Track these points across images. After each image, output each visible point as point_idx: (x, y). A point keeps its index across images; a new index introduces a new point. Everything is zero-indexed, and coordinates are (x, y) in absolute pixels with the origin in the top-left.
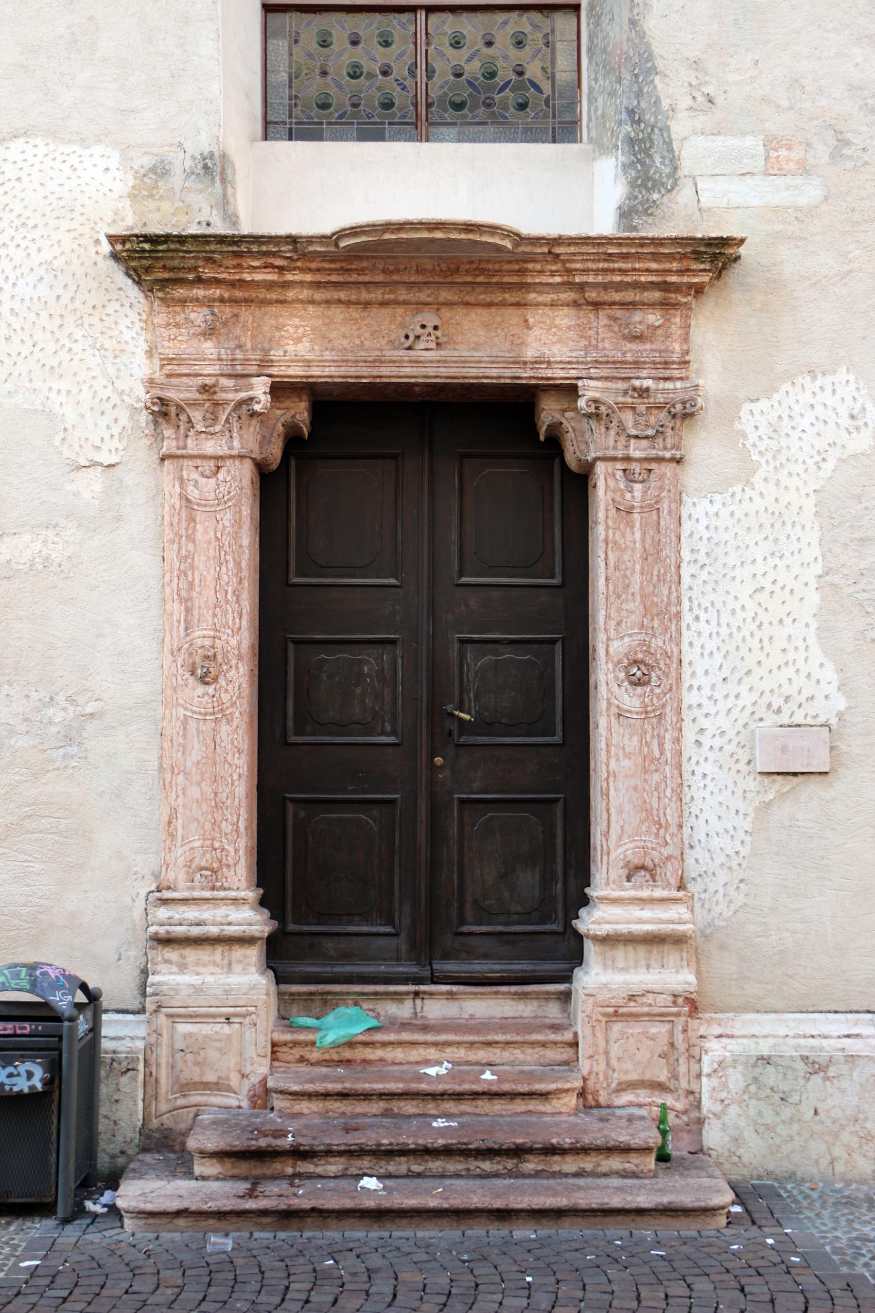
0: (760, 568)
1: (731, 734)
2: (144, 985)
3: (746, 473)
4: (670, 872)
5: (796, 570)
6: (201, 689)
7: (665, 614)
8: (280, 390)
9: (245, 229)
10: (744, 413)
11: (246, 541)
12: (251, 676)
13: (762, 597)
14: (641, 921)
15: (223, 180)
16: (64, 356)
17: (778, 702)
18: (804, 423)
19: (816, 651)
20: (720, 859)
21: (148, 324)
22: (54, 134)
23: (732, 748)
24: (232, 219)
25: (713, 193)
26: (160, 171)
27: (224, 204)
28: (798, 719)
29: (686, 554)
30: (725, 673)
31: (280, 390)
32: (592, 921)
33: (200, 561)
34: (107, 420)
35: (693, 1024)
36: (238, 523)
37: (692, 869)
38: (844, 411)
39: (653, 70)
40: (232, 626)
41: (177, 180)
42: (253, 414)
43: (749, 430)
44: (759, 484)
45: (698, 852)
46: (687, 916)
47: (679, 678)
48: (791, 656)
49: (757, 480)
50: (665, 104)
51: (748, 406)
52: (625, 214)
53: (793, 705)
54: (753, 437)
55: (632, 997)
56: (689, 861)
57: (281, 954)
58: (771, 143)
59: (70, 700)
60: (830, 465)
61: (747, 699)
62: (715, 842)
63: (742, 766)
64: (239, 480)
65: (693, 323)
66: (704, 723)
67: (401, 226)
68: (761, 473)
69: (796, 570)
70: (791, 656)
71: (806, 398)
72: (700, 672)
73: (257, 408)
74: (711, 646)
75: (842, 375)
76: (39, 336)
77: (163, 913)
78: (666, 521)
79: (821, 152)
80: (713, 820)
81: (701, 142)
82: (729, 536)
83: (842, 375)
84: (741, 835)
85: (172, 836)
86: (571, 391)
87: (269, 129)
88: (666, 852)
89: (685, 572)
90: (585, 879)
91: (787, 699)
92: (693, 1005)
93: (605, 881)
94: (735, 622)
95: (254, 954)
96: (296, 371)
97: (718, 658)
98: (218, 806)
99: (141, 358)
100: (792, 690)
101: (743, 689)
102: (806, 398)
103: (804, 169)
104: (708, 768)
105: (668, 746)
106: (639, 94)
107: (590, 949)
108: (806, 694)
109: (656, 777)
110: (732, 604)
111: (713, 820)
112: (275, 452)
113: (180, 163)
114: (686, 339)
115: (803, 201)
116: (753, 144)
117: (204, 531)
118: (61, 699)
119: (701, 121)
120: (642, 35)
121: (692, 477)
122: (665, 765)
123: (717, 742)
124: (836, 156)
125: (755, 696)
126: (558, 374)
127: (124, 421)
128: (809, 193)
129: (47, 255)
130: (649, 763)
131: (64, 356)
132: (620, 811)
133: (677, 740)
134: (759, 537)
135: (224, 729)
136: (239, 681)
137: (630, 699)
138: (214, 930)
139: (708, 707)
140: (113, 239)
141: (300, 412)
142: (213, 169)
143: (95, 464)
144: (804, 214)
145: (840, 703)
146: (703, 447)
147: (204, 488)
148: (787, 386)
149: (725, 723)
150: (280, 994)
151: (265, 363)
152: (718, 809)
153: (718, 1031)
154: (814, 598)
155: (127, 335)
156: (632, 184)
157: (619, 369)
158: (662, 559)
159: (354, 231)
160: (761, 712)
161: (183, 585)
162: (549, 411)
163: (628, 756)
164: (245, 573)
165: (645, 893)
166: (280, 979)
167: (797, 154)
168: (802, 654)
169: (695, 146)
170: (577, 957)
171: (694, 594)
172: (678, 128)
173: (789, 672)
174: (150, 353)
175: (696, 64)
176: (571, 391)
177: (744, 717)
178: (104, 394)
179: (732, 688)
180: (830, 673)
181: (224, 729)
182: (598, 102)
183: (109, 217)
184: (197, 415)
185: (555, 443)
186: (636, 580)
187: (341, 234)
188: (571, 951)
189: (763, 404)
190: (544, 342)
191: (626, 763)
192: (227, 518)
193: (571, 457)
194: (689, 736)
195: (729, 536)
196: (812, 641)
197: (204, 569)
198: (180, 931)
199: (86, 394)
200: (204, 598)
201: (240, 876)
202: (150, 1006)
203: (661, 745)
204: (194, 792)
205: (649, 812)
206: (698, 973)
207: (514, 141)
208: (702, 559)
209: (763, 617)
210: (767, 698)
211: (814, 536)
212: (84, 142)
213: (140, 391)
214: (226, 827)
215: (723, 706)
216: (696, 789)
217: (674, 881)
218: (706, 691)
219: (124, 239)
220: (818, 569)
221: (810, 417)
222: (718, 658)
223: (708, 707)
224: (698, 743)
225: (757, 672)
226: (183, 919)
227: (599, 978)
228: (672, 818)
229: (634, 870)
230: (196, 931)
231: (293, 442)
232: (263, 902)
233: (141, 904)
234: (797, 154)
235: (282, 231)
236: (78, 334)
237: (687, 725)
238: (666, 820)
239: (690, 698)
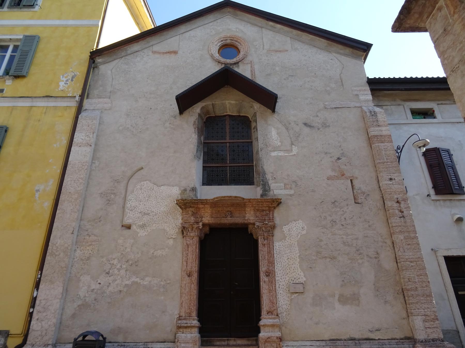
0: (288, 254)
1: (285, 285)
2: (175, 336)
3: (285, 238)
4: (275, 313)
5: (295, 255)
6: (188, 278)
7: (271, 263)
8: (204, 225)
9: (199, 198)
10: (284, 228)
11: (197, 251)
12: (197, 284)
13: (289, 260)
14: (270, 322)
15: (195, 191)
16: (167, 220)
17: (293, 279)
18: (294, 229)
19: (299, 269)
20: (284, 310)
21: (182, 215)
22: (168, 185)
23: (285, 288)
24: (197, 197)
25: (276, 192)
26: (185, 190)
27: (196, 195)
28: (297, 282)
29: (275, 252)
30: (283, 274)
31: (204, 225)
32: (262, 323)
33: (189, 254)
34: (174, 230)
35: (281, 343)
36: (196, 248)
37: (279, 312)
38: (301, 227)
39: (266, 174)
40: (194, 266)
41: (188, 191)
42: (199, 229)
43: (285, 230)
44: (287, 240)
45: (280, 308)
46: (279, 321)
47: (275, 275)
48: (295, 270)
49: (287, 239)
50: (268, 179)
51: (284, 226)
52: (262, 196)
53: (296, 280)
54: (285, 232)
55: (269, 338)
56: (279, 310)
57: (202, 331)
58: (285, 184)
59: (165, 280)
60: (299, 236)
61: (287, 279)
62: (283, 306)
63: (287, 291)
64: (196, 240)
65: (277, 220)
66: (280, 283)
67: (224, 197)
68: (287, 238)
69: (295, 255)
70: (295, 270)
71: (294, 225)
72: (279, 274)
73: (200, 228)
74: (280, 269)
75: (300, 221)
76: (163, 217)
77: (180, 322)
78: (271, 246)
79: (293, 186)
80: (283, 302)
81: (274, 184)
82: (282, 249)
83: (300, 221)
84: (288, 305)
85: (182, 306)
86: (254, 224)
87: (204, 184)
88: (274, 308)
89: (275, 255)
90: (260, 315)
91: (295, 278)
92: (281, 339)
93: (264, 313)
94: (285, 264)
95: (196, 330)
96: (207, 222)
97: (282, 271)
98: (191, 300)
99: (181, 220)
100: (296, 277)
101: (287, 277)
102: (294, 225)
103: (291, 189)
104: (281, 292)
105: (274, 287)
106: (263, 177)
107: (262, 328)
108: (298, 277)
109: (272, 294)
110: (284, 261)
111: (283, 302)
112: (203, 235)
113: (188, 189)
114: (273, 215)
115: (291, 193)
116: (282, 185)
117: (190, 249)
118: (163, 280)
119: (273, 181)
120: (263, 169)
121: (275, 238)
122: (273, 291)
123: (283, 287)
124: (296, 186)
125: (289, 278)
126: (251, 221)
127: (177, 230)
128: (292, 192)
129: (166, 204)
130: (270, 291)
131: (167, 220)
132: (265, 300)
133: (275, 286)
134: (288, 249)
135: (193, 285)
136: (195, 276)
137: (266, 279)
138: (189, 325)
139: (281, 280)
140: (177, 200)
141: (207, 229)
142: (194, 189)
143: (171, 238)
144: (291, 195)
145: (305, 279)
146: (277, 233)
147: (190, 241)
148: (291, 223)
149: (284, 283)
150: (201, 340)
151: (201, 221)
152: (283, 300)
153: (286, 345)
154: (298, 260)
155: (178, 216)
156: (263, 191)
157: (263, 221)
158: (270, 253)
159: (217, 198)
160: (290, 281)
161: (186, 259)
162: (250, 226)
163: (266, 289)
164: (197, 257)
165: (270, 317)
166: (202, 337)
167: (290, 186)
168: (297, 270)
169: (273, 185)
170: (259, 332)
171: (277, 259)
172: (270, 183)
173: (295, 273)
174: (182, 219)
175: (272, 173)
176: (254, 224)
177: (287, 282)
178: (174, 226)
179: (285, 276)
180: (302, 274)
181: (193, 285)
182: (256, 178)
183: (176, 197)
184: (190, 229)
185: (251, 234)
186: (266, 257)
187: (214, 199)
188: (258, 331)
189: (287, 226)
190: (250, 216)
191: (266, 291)
192: (194, 247)
193: (255, 237)
194: (277, 286)
195: (282, 249)
196: (298, 267)
197: (190, 256)
198: (183, 325)
199: (171, 226)
200: (190, 261)
201: (194, 314)
202: (176, 341)
203: (272, 286)
204: (187, 298)
205: (271, 301)
206: (281, 333)
207: (244, 185)
208: (278, 253)
209: (289, 263)
210: (291, 278)
211: (297, 249)
212: (173, 186)
213: (180, 226)
214: (192, 304)
215: (283, 280)
216: (279, 296)
217: (276, 314)
218: (280, 277)
219: (179, 200)
220: (299, 255)
221: (295, 228)
222: (282, 271)
223: (281, 280)
224: (279, 287)
225: (289, 274)
226: (183, 323)
227: (263, 335)
228: (275, 302)
229: (268, 313)
230: (186, 325)
231: (206, 235)
232: (199, 321)
233: (176, 320)
234: (290, 186)
235: (204, 198)
236: (170, 216)
237: (277, 284)
238: (274, 302)
239: (277, 279)
